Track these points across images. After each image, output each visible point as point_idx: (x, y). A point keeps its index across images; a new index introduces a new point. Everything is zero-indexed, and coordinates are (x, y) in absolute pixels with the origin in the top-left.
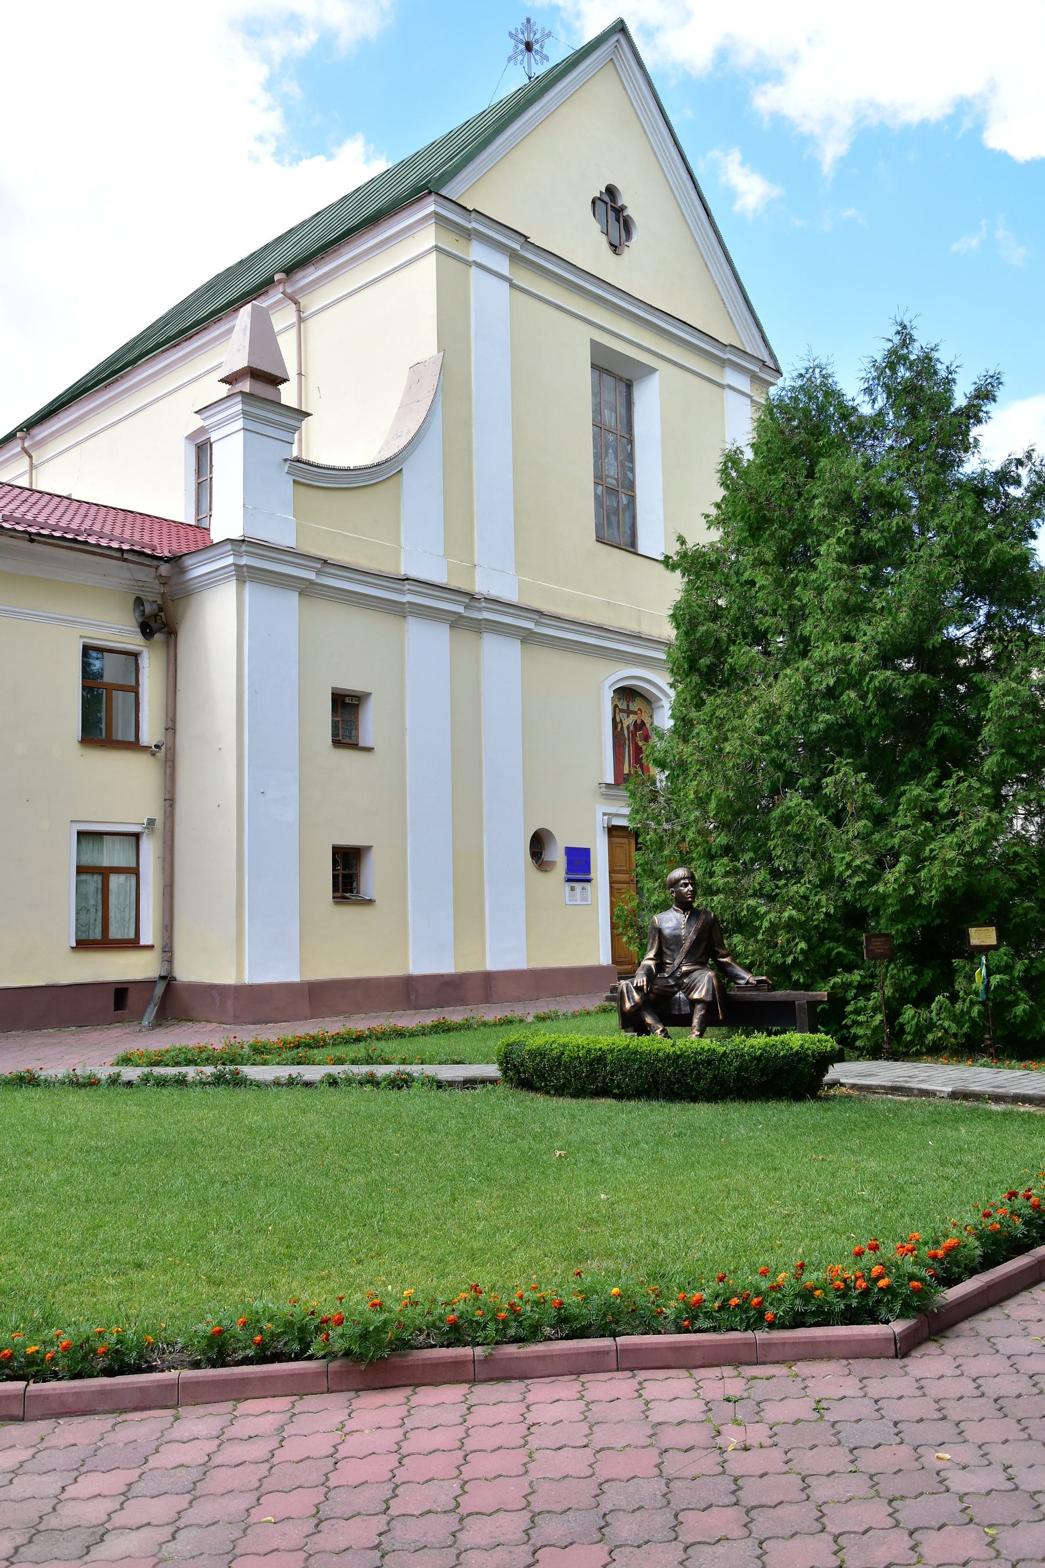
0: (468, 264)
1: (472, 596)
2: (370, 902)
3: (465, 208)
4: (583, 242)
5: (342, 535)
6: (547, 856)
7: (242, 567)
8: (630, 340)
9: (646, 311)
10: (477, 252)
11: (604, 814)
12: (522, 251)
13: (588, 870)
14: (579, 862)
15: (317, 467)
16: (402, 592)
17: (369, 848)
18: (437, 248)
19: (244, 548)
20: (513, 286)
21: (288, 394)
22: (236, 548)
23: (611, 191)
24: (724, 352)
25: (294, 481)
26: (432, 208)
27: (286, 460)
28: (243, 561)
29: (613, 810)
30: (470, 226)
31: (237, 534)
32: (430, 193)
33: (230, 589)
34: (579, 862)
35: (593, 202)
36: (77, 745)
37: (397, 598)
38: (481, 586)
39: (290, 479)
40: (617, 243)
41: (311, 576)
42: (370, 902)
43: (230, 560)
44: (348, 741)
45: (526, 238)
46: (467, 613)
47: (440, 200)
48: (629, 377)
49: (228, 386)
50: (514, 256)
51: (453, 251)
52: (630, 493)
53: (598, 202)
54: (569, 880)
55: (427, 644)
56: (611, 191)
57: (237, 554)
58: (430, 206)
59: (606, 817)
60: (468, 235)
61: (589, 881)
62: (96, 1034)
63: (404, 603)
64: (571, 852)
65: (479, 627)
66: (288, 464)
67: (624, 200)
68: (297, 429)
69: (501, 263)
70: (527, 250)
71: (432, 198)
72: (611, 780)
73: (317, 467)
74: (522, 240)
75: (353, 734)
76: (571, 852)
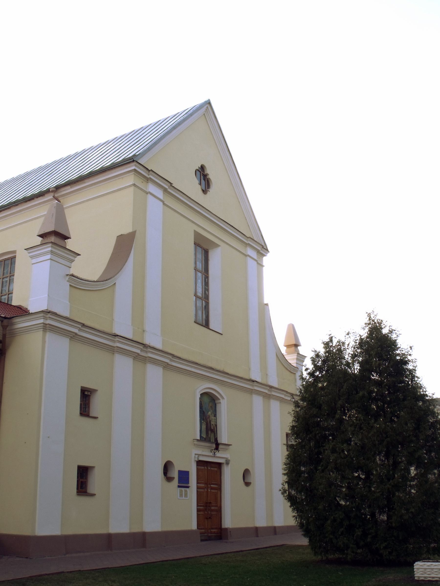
0: (147, 193)
1: (145, 345)
2: (93, 495)
3: (147, 169)
4: (191, 187)
5: (89, 312)
6: (170, 475)
7: (46, 324)
8: (211, 232)
9: (217, 220)
10: (152, 188)
11: (196, 454)
12: (169, 188)
13: (188, 482)
14: (184, 477)
15: (81, 279)
16: (114, 341)
17: (93, 467)
18: (134, 185)
19: (49, 315)
20: (164, 204)
21: (70, 244)
22: (45, 315)
23: (202, 168)
24: (247, 240)
25: (70, 285)
26: (134, 168)
27: (67, 275)
28: (49, 322)
29: (200, 452)
30: (148, 177)
31: (44, 308)
32: (134, 161)
33: (40, 333)
34: (184, 477)
35: (196, 171)
36: (289, 323)
37: (110, 343)
38: (148, 341)
39: (68, 284)
40: (204, 189)
41: (76, 331)
42: (93, 495)
43: (42, 321)
44: (85, 413)
45: (171, 184)
46: (141, 353)
47: (137, 165)
48: (207, 248)
49: (41, 239)
50: (165, 190)
51: (142, 188)
52: (207, 301)
53: (197, 172)
54: (179, 487)
55: (123, 367)
56: (202, 168)
57: (45, 318)
58: (132, 167)
59: (197, 456)
60: (148, 180)
61: (188, 487)
62: (225, 476)
63: (114, 347)
64: (180, 472)
65: (145, 360)
66: (68, 276)
67: (208, 171)
68: (73, 261)
69: (159, 193)
70: (171, 189)
71: (135, 163)
72: (199, 438)
73: (81, 279)
74: (169, 185)
75: (87, 410)
76: (180, 472)
